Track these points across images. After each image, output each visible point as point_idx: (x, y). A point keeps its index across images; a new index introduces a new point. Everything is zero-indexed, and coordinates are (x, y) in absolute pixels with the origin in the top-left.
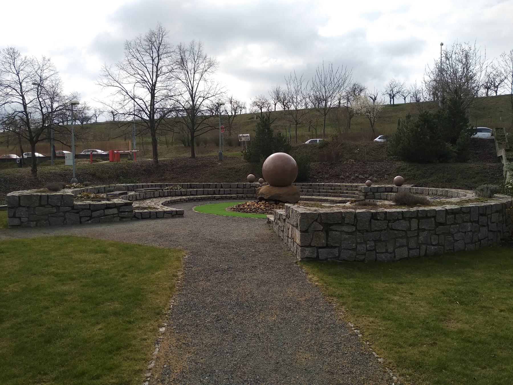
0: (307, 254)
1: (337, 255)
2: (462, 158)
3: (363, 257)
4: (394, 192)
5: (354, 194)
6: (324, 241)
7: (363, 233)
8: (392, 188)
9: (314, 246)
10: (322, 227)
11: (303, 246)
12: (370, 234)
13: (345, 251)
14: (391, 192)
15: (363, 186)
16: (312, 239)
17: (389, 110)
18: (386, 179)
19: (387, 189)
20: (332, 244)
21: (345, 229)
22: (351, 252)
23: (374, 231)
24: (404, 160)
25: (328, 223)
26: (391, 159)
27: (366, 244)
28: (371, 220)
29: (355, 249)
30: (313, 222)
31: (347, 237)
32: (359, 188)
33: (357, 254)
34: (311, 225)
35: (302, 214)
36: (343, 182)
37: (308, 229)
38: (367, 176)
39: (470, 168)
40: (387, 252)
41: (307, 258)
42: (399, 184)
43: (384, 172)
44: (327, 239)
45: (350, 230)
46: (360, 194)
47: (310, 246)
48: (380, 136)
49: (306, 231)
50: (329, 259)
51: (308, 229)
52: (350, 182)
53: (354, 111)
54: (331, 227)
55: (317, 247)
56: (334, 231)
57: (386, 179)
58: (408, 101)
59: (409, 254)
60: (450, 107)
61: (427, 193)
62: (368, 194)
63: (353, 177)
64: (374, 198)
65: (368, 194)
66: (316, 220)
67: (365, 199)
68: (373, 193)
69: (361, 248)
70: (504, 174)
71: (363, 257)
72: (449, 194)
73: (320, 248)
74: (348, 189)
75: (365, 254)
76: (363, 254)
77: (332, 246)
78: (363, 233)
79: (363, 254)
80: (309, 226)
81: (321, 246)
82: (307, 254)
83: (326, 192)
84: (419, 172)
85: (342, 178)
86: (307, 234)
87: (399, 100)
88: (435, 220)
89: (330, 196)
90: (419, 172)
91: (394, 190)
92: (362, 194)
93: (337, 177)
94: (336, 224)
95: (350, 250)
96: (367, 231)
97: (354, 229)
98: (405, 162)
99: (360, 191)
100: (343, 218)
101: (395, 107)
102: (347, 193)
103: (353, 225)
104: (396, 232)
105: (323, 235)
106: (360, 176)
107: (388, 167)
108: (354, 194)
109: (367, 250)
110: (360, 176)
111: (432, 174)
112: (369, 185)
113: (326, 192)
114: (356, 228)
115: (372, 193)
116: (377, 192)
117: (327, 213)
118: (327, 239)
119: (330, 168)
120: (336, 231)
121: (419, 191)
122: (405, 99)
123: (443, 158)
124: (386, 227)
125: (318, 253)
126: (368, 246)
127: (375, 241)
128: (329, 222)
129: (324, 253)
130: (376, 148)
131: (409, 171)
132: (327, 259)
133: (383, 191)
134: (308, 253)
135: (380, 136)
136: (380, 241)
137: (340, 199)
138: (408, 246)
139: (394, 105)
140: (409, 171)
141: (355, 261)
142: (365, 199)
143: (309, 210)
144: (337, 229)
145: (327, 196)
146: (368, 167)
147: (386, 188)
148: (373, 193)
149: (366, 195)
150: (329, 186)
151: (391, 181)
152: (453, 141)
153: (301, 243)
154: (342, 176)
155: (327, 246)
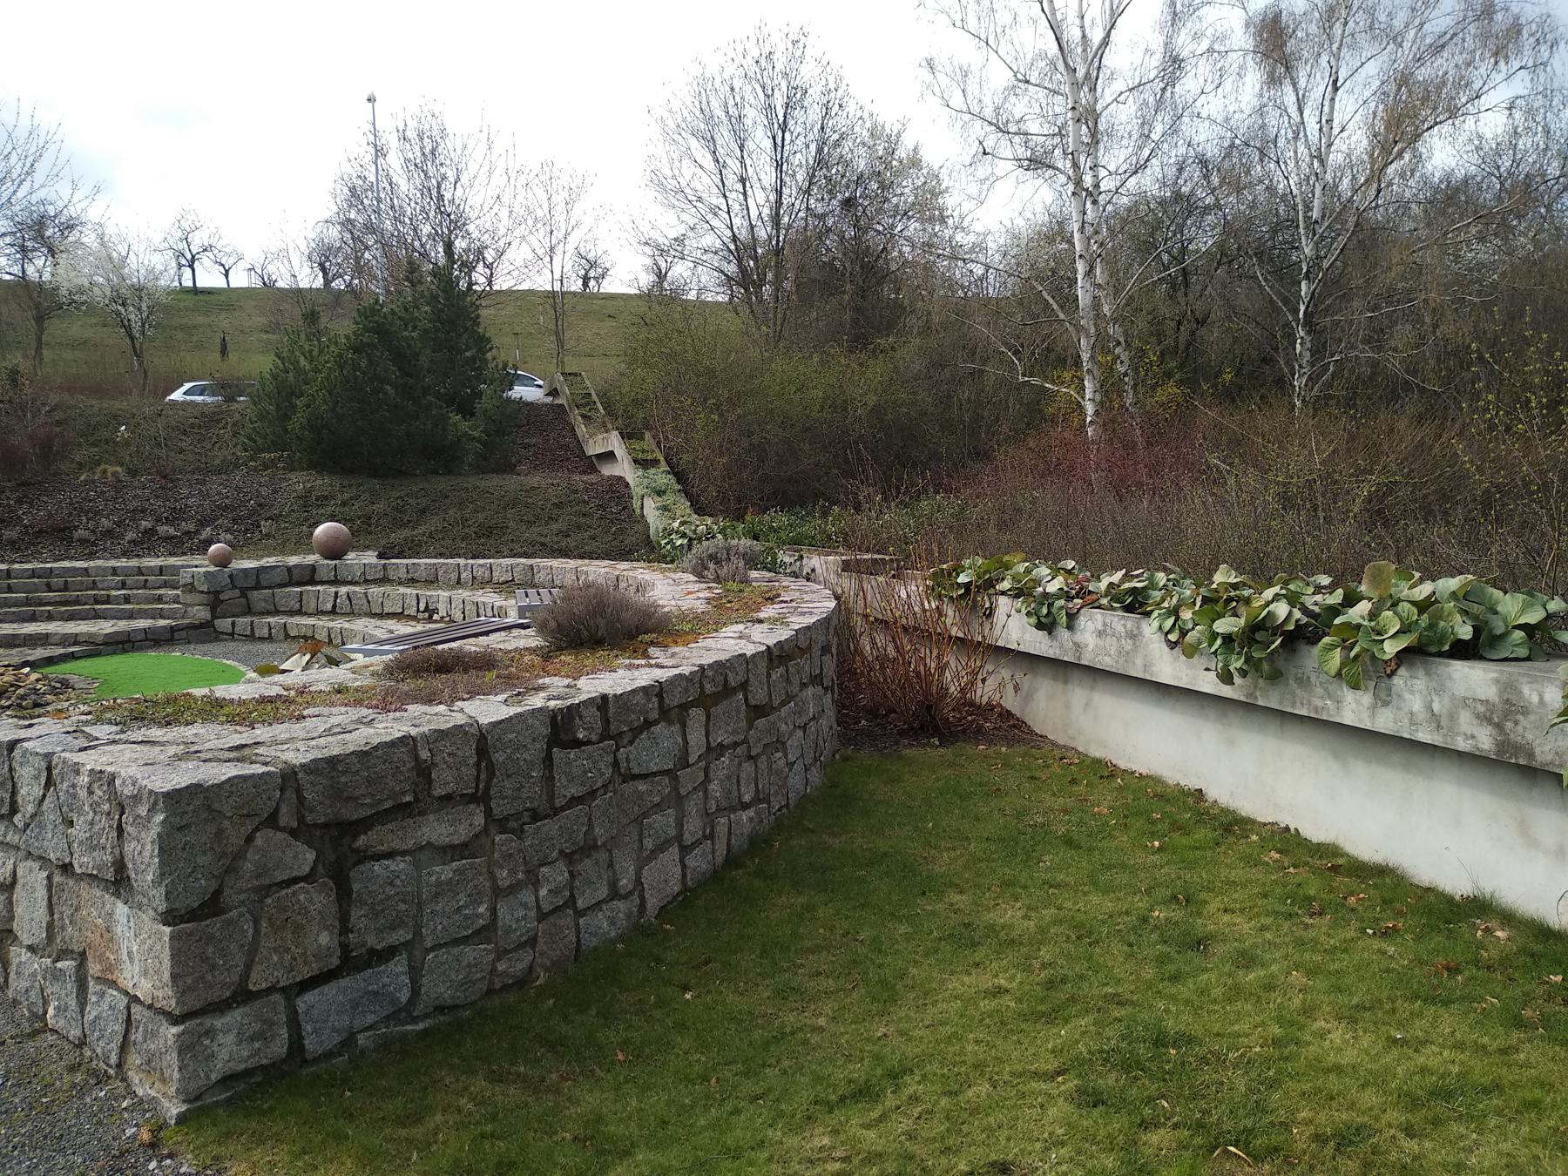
0: (224, 1054)
1: (404, 996)
2: (497, 460)
3: (526, 957)
4: (322, 583)
5: (160, 599)
6: (324, 939)
7: (519, 833)
8: (313, 568)
9: (270, 990)
10: (311, 856)
11: (196, 1010)
12: (550, 827)
13: (443, 955)
14: (312, 582)
15: (198, 566)
16: (252, 951)
17: (182, 304)
18: (268, 536)
19: (295, 572)
20: (372, 941)
21: (437, 829)
22: (470, 953)
23: (563, 809)
24: (312, 465)
25: (336, 816)
26: (271, 465)
27: (536, 884)
28: (548, 759)
29: (486, 933)
30: (249, 839)
31: (446, 872)
32: (185, 577)
33: (501, 954)
34: (240, 855)
35: (175, 799)
36: (91, 556)
37: (218, 893)
38: (191, 527)
39: (533, 489)
40: (615, 894)
41: (227, 1080)
42: (334, 551)
43: (253, 513)
44: (344, 918)
45: (462, 833)
46: (189, 598)
47: (243, 995)
48: (187, 386)
49: (212, 906)
50: (361, 1039)
51: (218, 893)
52: (126, 554)
53: (64, 291)
54: (361, 841)
55: (284, 990)
56: (378, 857)
57: (268, 536)
58: (239, 280)
59: (684, 875)
60: (434, 297)
61: (454, 576)
62: (222, 597)
63: (130, 535)
64: (249, 611)
65: (222, 597)
66: (272, 821)
67: (214, 617)
68: (244, 592)
69: (515, 915)
70: (636, 504)
71: (526, 957)
72: (540, 577)
73: (305, 986)
74: (130, 581)
75: (532, 942)
76: (521, 946)
77: (372, 952)
78: (519, 833)
79: (521, 946)
80: (230, 870)
81: (314, 969)
82: (224, 1054)
83: (28, 602)
84: (380, 507)
85: (83, 541)
86: (214, 925)
87: (209, 278)
88: (746, 699)
89: (50, 618)
90: (380, 507)
91: (322, 574)
92: (197, 598)
93: (59, 536)
94: (383, 817)
95: (465, 940)
96: (536, 816)
97: (479, 820)
98: (320, 472)
99: (190, 588)
100: (424, 772)
101: (201, 297)
102: (127, 600)
103: (472, 799)
104: (642, 786)
105: (317, 899)
106: (163, 529)
107: (264, 491)
108: (160, 599)
109: (542, 916)
110: (163, 529)
111: (424, 511)
112: (222, 562)
113: (28, 602)
114: (488, 813)
115: (237, 592)
116: (258, 587)
117: (332, 762)
118: (344, 918)
119: (19, 501)
120: (390, 855)
121: (421, 574)
122: (227, 276)
123: (442, 457)
124: (609, 772)
125: (294, 1022)
126: (543, 892)
127: (569, 857)
128: (352, 813)
129: (328, 1013)
130: (192, 426)
131: (344, 504)
132: (349, 1041)
133: (278, 580)
134: (230, 1045)
135: (187, 386)
136: (588, 848)
137: (106, 627)
138: (679, 838)
139: (195, 290)
140: (344, 504)
141: (490, 992)
142: (214, 617)
143: (190, 753)
144: (397, 845)
145: (33, 618)
146: (185, 491)
147: (289, 569)
148: (244, 592)
149: (215, 602)
150: (34, 574)
151: (303, 543)
152: (467, 411)
153: (182, 991)
154: (81, 533)
155: (350, 962)
